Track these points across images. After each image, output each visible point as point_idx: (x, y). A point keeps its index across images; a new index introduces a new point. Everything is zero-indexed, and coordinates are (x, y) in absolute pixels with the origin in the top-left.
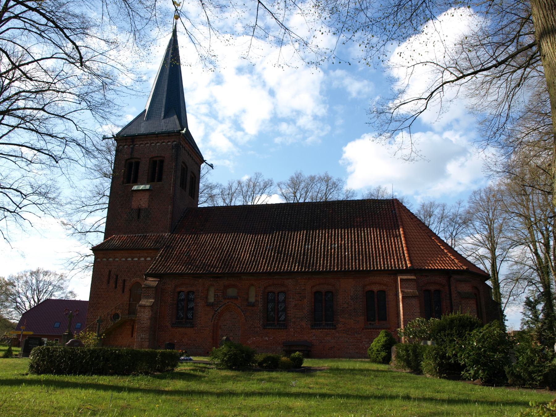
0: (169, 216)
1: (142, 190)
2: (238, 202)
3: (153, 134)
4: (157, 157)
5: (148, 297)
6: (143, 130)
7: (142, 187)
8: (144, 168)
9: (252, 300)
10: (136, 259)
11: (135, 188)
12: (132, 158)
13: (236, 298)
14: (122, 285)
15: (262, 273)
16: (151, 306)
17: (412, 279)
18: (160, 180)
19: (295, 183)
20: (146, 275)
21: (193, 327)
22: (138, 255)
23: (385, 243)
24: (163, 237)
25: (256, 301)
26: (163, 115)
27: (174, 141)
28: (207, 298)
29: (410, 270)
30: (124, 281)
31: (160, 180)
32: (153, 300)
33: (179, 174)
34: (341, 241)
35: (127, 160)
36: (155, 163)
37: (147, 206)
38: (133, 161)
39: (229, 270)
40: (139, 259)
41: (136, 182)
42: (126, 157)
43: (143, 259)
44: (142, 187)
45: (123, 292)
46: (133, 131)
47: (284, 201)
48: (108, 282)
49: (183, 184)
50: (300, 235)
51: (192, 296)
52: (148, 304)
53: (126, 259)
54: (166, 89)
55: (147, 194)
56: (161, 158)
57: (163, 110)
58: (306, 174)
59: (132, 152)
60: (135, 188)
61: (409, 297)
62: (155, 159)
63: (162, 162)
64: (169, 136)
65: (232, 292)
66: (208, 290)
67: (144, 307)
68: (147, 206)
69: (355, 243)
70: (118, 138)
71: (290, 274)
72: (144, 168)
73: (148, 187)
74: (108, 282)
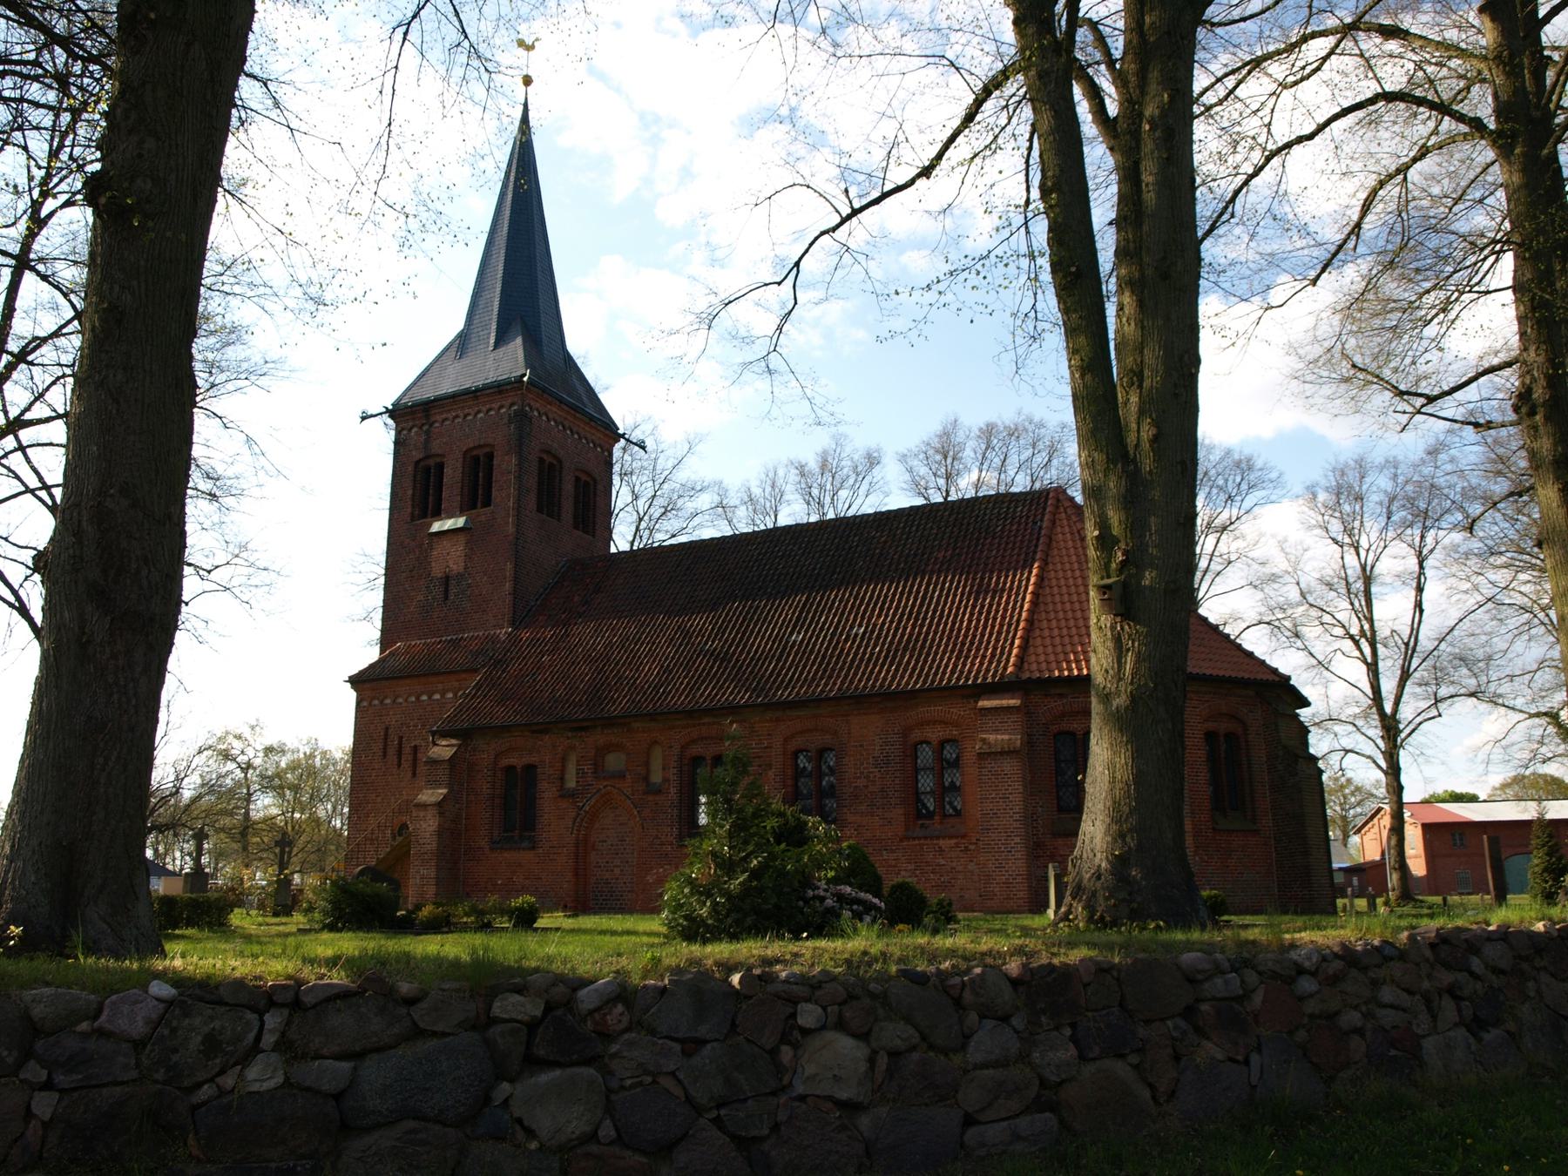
0: (508, 586)
1: (448, 531)
2: (793, 512)
3: (467, 392)
4: (480, 446)
5: (435, 784)
6: (447, 387)
7: (448, 524)
8: (453, 474)
9: (656, 777)
10: (437, 696)
11: (436, 527)
12: (427, 457)
13: (621, 776)
14: (410, 758)
15: (946, 688)
16: (439, 804)
17: (1008, 709)
18: (487, 503)
19: (945, 451)
20: (434, 734)
21: (533, 848)
22: (440, 686)
23: (980, 613)
24: (494, 640)
25: (666, 780)
26: (492, 341)
27: (512, 404)
28: (562, 779)
29: (1010, 682)
30: (415, 748)
31: (487, 503)
32: (445, 791)
33: (532, 481)
34: (879, 616)
35: (417, 462)
36: (476, 459)
37: (461, 570)
38: (431, 462)
39: (925, 682)
40: (443, 696)
41: (438, 514)
42: (417, 455)
43: (450, 695)
44: (448, 524)
45: (414, 774)
46: (428, 393)
47: (919, 501)
48: (385, 755)
49: (548, 502)
50: (788, 609)
51: (949, 753)
52: (433, 799)
53: (418, 698)
54: (500, 275)
55: (462, 538)
56: (487, 450)
57: (494, 326)
58: (973, 419)
59: (427, 441)
60: (436, 527)
61: (995, 753)
62: (475, 453)
63: (490, 456)
64: (500, 392)
65: (614, 761)
66: (564, 760)
67: (424, 806)
68: (461, 570)
69: (909, 619)
70: (398, 412)
71: (733, 710)
72: (453, 474)
73: (460, 522)
74: (385, 755)
